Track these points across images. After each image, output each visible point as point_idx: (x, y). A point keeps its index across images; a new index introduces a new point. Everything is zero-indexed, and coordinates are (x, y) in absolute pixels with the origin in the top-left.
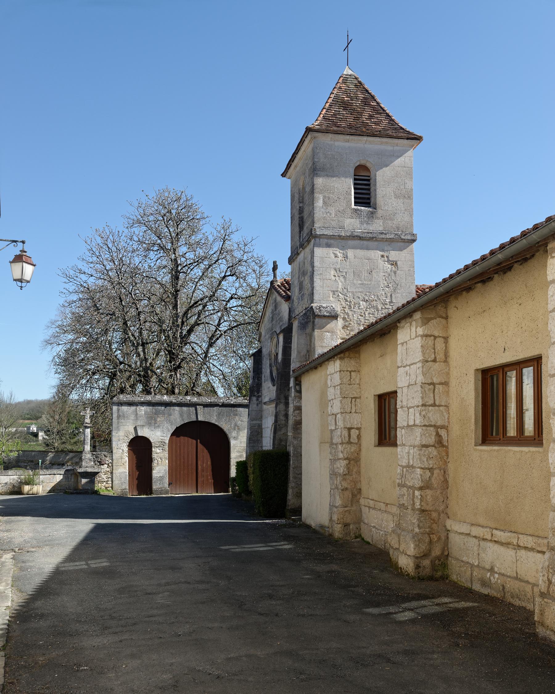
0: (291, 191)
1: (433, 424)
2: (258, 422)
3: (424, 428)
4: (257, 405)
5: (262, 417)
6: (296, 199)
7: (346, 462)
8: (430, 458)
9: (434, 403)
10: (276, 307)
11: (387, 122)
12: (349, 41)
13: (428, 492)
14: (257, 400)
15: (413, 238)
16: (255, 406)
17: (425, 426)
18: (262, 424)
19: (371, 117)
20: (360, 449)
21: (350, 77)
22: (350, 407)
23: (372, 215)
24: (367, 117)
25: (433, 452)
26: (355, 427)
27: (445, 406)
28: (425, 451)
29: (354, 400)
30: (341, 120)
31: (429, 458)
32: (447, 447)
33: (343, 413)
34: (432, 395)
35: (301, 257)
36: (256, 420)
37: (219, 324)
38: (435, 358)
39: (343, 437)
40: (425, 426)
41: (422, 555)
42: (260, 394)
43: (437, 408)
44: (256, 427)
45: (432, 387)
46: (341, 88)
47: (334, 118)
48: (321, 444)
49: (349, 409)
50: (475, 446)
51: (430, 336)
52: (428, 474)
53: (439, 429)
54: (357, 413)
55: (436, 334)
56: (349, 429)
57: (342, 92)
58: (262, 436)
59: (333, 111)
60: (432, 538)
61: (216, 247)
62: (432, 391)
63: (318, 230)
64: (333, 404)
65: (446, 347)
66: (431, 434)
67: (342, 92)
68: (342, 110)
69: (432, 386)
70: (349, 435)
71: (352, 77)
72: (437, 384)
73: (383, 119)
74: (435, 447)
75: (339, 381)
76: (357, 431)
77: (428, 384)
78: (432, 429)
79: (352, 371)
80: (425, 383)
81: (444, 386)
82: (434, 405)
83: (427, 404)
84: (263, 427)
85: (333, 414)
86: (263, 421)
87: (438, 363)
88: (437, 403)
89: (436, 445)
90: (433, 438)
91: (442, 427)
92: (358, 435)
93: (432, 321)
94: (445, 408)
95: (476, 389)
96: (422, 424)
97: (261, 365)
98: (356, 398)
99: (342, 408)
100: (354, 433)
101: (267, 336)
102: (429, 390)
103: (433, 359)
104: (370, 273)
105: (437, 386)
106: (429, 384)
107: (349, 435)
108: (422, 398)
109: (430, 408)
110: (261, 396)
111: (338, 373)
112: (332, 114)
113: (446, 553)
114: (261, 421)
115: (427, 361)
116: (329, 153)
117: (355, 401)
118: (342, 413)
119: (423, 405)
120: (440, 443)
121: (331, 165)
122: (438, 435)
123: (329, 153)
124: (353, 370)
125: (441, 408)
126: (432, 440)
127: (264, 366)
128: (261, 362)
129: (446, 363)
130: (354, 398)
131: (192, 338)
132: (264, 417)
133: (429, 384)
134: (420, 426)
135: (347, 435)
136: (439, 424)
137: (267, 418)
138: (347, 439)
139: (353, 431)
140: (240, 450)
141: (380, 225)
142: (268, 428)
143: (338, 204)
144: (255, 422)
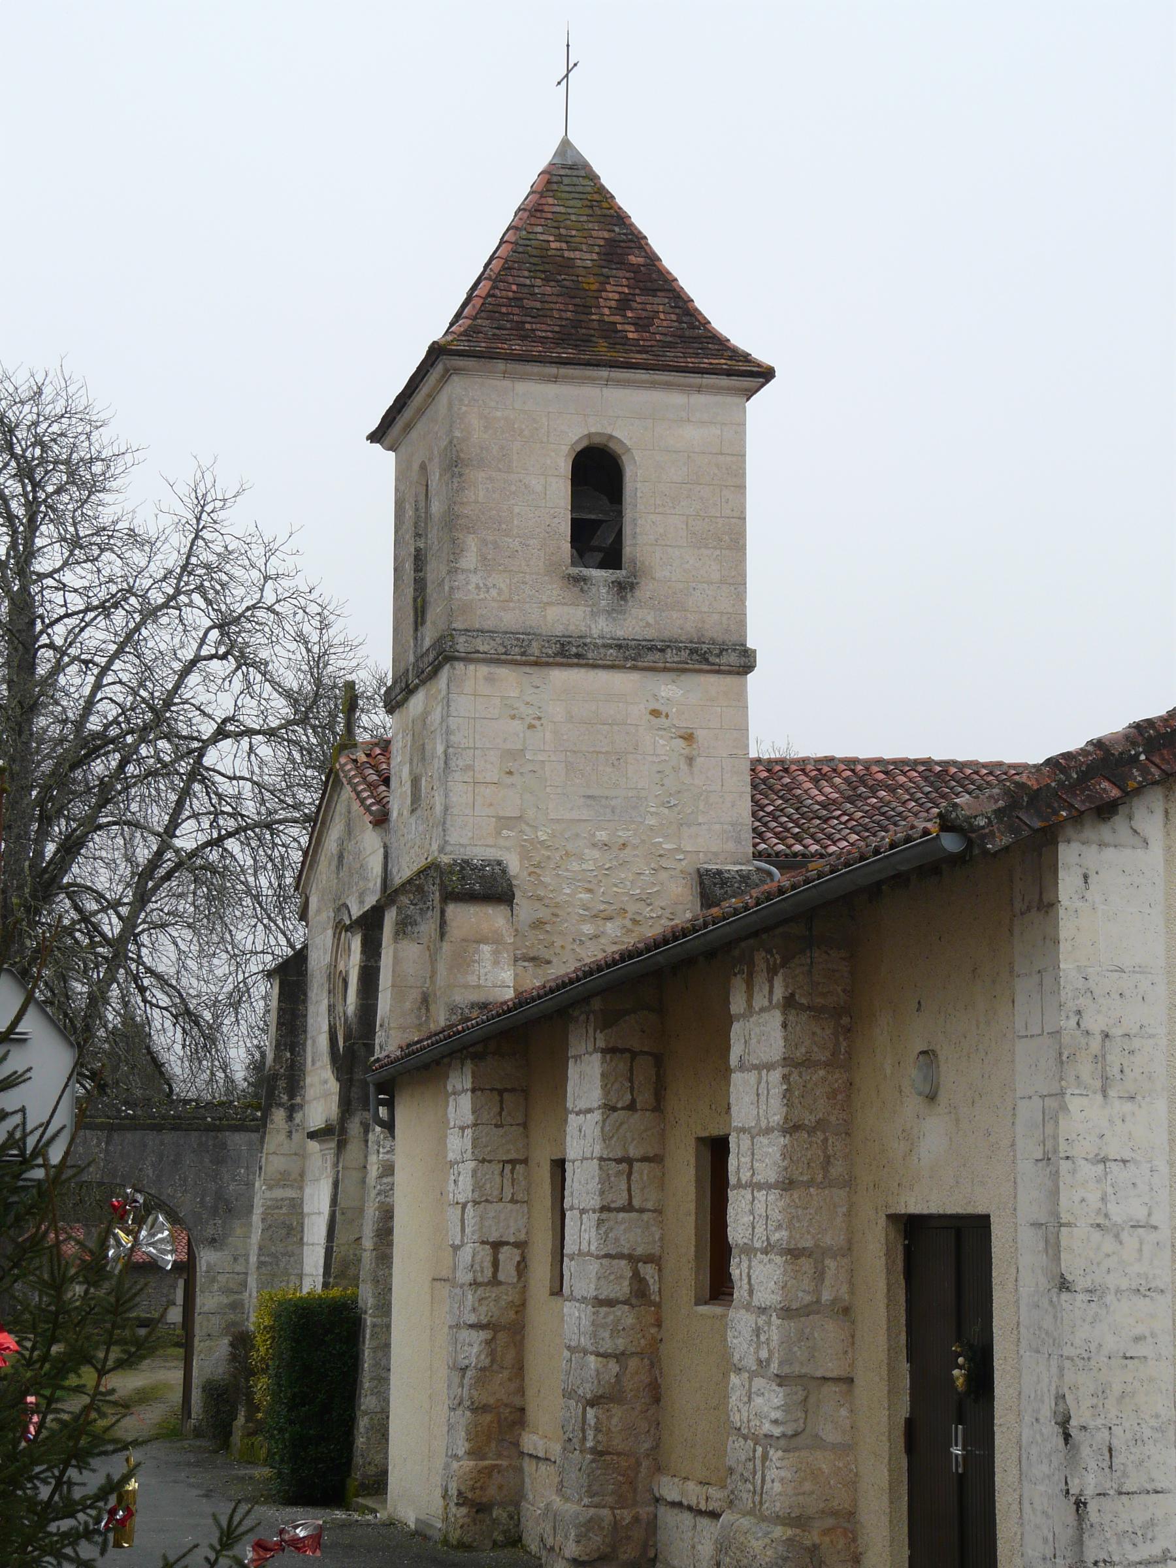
0: (397, 490)
1: (626, 1251)
2: (290, 1193)
3: (605, 1261)
4: (290, 1134)
5: (302, 1175)
6: (409, 524)
7: (484, 1335)
8: (619, 1331)
9: (630, 1203)
10: (349, 831)
11: (674, 317)
12: (570, 66)
13: (617, 1411)
14: (290, 1118)
15: (743, 661)
16: (282, 1137)
17: (607, 1256)
18: (302, 1199)
19: (624, 303)
20: (525, 1300)
21: (568, 172)
22: (498, 1186)
23: (624, 589)
24: (613, 304)
25: (625, 1316)
26: (512, 1240)
27: (654, 1211)
28: (606, 1315)
29: (508, 1167)
30: (539, 315)
31: (615, 1332)
32: (658, 1305)
33: (479, 1203)
34: (624, 1186)
35: (417, 703)
36: (284, 1186)
37: (171, 830)
38: (633, 1101)
39: (477, 1267)
40: (607, 1256)
41: (596, 1556)
42: (298, 1100)
43: (634, 1215)
44: (284, 1210)
45: (624, 1166)
46: (542, 211)
47: (516, 310)
48: (435, 1283)
49: (496, 1193)
50: (696, 1304)
51: (623, 1051)
52: (614, 1367)
53: (640, 1264)
54: (517, 1202)
55: (637, 1047)
56: (496, 1246)
57: (542, 222)
58: (302, 1239)
59: (514, 287)
60: (618, 1517)
61: (169, 557)
62: (625, 1177)
63: (462, 639)
64: (459, 1174)
65: (658, 1075)
66: (621, 1277)
67: (542, 222)
68: (538, 282)
69: (624, 1165)
70: (495, 1264)
71: (575, 173)
72: (638, 1160)
73: (661, 308)
74: (632, 1306)
75: (471, 1117)
76: (517, 1252)
77: (615, 1160)
78: (623, 1262)
79: (506, 1090)
80: (610, 1159)
81: (652, 1164)
82: (629, 1208)
83: (613, 1205)
84: (306, 1210)
85: (457, 1203)
86: (308, 1191)
87: (639, 1113)
88: (636, 1203)
89: (634, 1301)
90: (626, 1283)
91: (649, 1259)
92: (519, 1263)
93: (627, 1018)
94: (655, 1215)
95: (699, 1181)
96: (602, 1253)
97: (305, 1001)
98: (514, 1162)
99: (477, 1187)
100: (509, 1256)
101: (324, 915)
102: (619, 1174)
103: (628, 1102)
104: (616, 763)
105: (636, 1166)
106: (619, 1161)
107: (495, 1264)
108: (602, 1193)
109: (621, 1215)
110: (301, 1106)
111: (469, 1093)
112: (510, 294)
113: (652, 1555)
114: (301, 1188)
115: (614, 1109)
116: (499, 414)
117: (512, 1172)
118: (476, 1203)
119: (603, 1209)
120: (640, 1292)
121: (502, 448)
122: (637, 1278)
123: (499, 414)
124: (509, 1087)
125: (646, 1216)
126: (622, 1289)
127: (311, 1009)
128: (305, 994)
129: (657, 1114)
130: (508, 1162)
131: (78, 872)
132: (309, 1176)
133: (619, 1161)
134: (598, 1257)
135: (487, 1264)
136: (639, 1251)
137: (318, 1180)
138: (489, 1273)
139: (505, 1250)
140: (231, 1285)
141: (647, 623)
142: (319, 1213)
143: (523, 563)
144: (279, 1193)
